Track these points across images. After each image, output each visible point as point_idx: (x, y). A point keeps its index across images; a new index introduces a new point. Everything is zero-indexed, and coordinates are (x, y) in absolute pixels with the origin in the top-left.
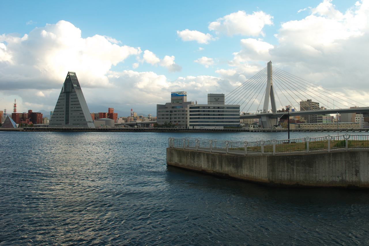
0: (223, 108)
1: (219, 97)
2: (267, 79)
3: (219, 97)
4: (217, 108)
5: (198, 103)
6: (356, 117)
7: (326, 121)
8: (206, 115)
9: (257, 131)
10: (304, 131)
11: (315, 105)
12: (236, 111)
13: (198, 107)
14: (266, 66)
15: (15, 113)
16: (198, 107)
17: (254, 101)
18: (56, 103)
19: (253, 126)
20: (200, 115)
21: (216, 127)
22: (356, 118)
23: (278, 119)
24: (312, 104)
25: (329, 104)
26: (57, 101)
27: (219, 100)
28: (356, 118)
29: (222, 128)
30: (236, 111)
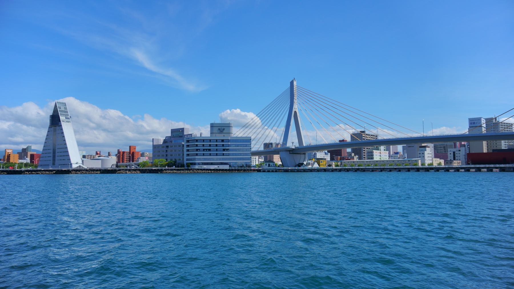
0: (228, 141)
1: (224, 128)
2: (290, 104)
3: (224, 128)
4: (221, 141)
5: (203, 136)
6: (419, 152)
7: (380, 157)
8: (206, 151)
9: (274, 171)
10: (338, 170)
11: (367, 137)
12: (246, 145)
13: (208, 164)
14: (289, 85)
15: (220, 137)
16: (208, 164)
17: (268, 134)
18: (45, 140)
19: (267, 164)
20: (199, 150)
21: (218, 166)
22: (420, 154)
23: (320, 157)
24: (367, 137)
25: (423, 133)
26: (45, 138)
27: (224, 132)
28: (420, 154)
29: (227, 167)
30: (246, 145)
